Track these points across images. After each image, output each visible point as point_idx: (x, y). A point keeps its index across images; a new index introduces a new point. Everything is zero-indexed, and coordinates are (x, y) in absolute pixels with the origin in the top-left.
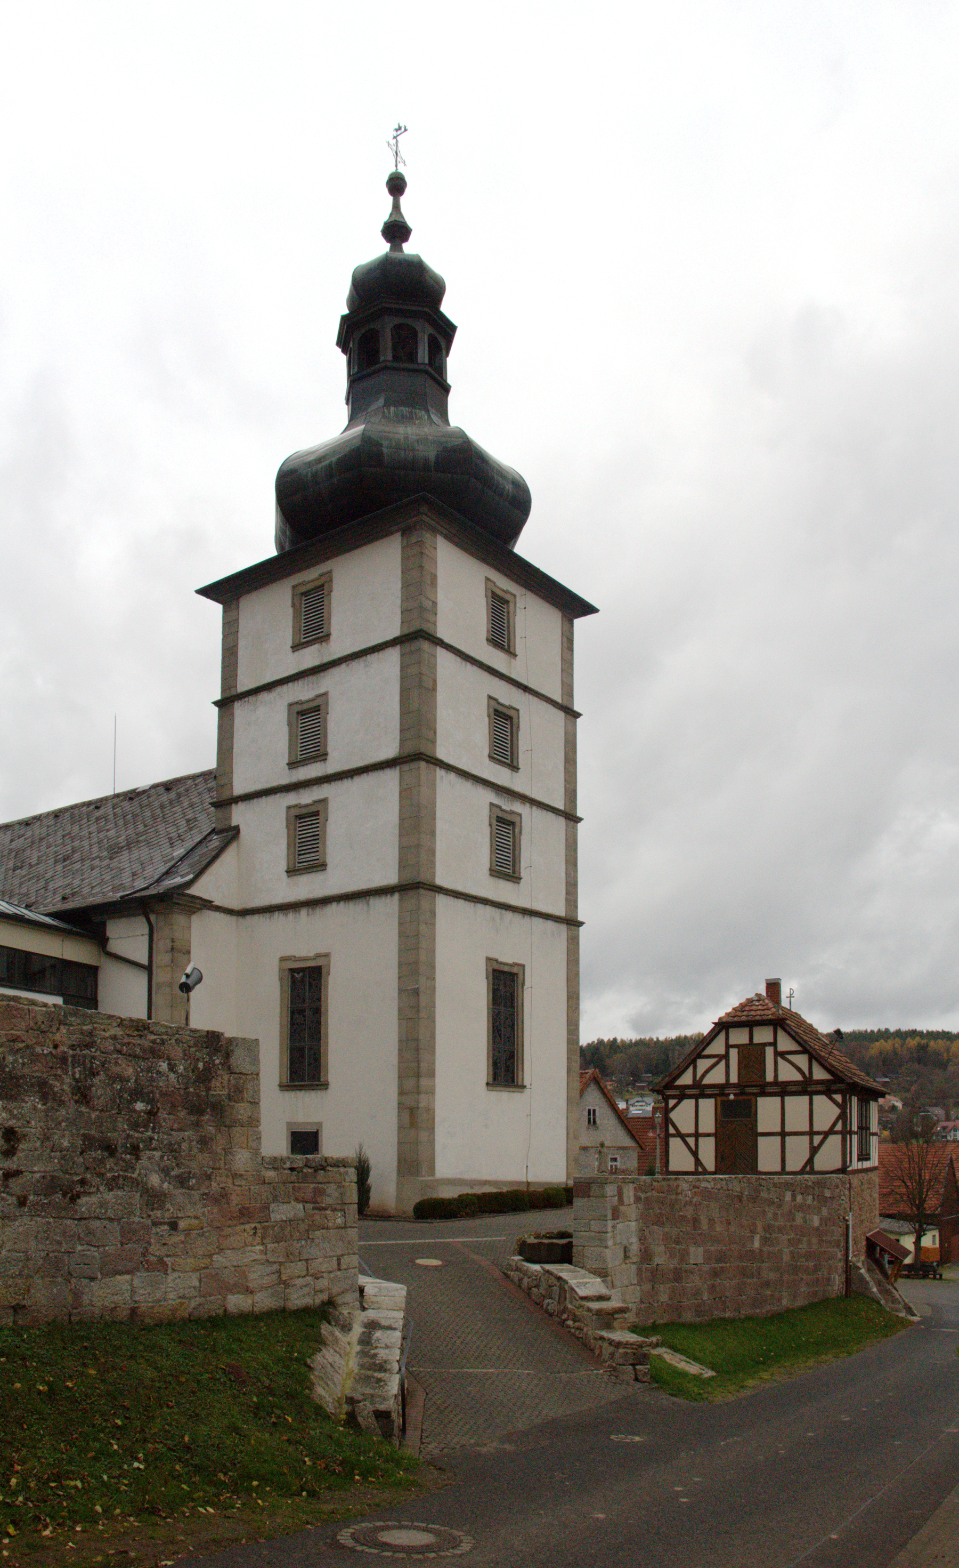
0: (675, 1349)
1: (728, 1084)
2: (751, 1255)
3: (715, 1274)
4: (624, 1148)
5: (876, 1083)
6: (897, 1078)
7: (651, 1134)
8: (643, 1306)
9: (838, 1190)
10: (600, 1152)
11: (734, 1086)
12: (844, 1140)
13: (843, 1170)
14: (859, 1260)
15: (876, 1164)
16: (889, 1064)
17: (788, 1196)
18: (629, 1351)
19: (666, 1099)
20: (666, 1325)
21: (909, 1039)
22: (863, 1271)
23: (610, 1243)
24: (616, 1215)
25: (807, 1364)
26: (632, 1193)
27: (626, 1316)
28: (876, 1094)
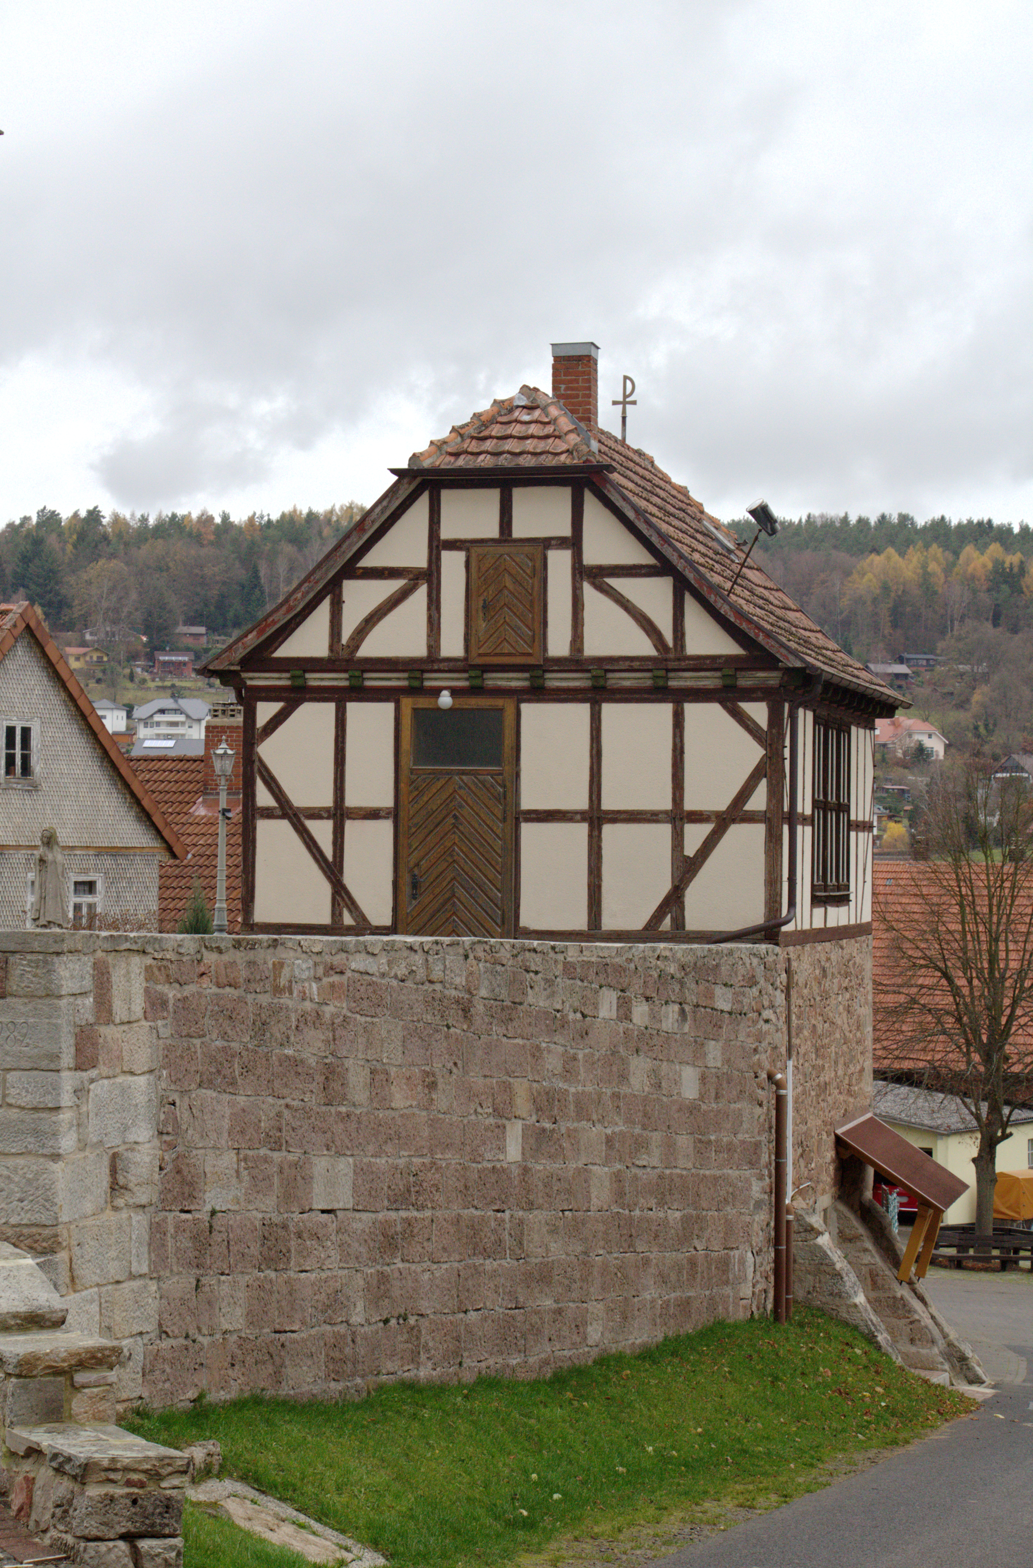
0: (260, 1483)
1: (433, 661)
2: (496, 1187)
3: (389, 1242)
4: (115, 852)
5: (875, 674)
6: (930, 666)
7: (200, 811)
8: (165, 1344)
9: (755, 991)
10: (42, 861)
11: (453, 665)
12: (773, 840)
13: (769, 932)
14: (815, 1205)
15: (867, 917)
16: (909, 621)
17: (607, 1005)
18: (119, 1491)
19: (249, 699)
20: (238, 1405)
21: (969, 550)
22: (824, 1240)
23: (67, 1142)
24: (87, 1054)
25: (660, 1529)
26: (138, 986)
27: (112, 1376)
28: (870, 707)
